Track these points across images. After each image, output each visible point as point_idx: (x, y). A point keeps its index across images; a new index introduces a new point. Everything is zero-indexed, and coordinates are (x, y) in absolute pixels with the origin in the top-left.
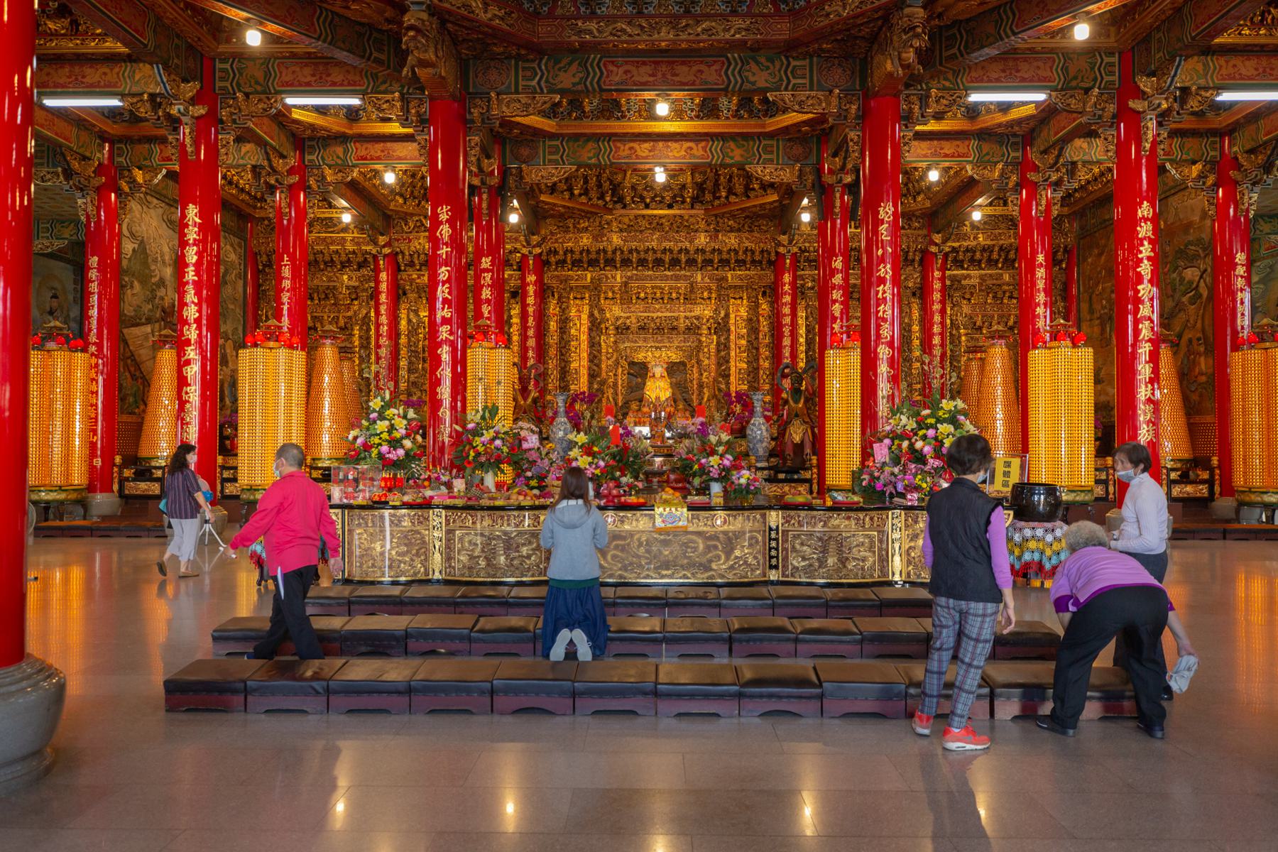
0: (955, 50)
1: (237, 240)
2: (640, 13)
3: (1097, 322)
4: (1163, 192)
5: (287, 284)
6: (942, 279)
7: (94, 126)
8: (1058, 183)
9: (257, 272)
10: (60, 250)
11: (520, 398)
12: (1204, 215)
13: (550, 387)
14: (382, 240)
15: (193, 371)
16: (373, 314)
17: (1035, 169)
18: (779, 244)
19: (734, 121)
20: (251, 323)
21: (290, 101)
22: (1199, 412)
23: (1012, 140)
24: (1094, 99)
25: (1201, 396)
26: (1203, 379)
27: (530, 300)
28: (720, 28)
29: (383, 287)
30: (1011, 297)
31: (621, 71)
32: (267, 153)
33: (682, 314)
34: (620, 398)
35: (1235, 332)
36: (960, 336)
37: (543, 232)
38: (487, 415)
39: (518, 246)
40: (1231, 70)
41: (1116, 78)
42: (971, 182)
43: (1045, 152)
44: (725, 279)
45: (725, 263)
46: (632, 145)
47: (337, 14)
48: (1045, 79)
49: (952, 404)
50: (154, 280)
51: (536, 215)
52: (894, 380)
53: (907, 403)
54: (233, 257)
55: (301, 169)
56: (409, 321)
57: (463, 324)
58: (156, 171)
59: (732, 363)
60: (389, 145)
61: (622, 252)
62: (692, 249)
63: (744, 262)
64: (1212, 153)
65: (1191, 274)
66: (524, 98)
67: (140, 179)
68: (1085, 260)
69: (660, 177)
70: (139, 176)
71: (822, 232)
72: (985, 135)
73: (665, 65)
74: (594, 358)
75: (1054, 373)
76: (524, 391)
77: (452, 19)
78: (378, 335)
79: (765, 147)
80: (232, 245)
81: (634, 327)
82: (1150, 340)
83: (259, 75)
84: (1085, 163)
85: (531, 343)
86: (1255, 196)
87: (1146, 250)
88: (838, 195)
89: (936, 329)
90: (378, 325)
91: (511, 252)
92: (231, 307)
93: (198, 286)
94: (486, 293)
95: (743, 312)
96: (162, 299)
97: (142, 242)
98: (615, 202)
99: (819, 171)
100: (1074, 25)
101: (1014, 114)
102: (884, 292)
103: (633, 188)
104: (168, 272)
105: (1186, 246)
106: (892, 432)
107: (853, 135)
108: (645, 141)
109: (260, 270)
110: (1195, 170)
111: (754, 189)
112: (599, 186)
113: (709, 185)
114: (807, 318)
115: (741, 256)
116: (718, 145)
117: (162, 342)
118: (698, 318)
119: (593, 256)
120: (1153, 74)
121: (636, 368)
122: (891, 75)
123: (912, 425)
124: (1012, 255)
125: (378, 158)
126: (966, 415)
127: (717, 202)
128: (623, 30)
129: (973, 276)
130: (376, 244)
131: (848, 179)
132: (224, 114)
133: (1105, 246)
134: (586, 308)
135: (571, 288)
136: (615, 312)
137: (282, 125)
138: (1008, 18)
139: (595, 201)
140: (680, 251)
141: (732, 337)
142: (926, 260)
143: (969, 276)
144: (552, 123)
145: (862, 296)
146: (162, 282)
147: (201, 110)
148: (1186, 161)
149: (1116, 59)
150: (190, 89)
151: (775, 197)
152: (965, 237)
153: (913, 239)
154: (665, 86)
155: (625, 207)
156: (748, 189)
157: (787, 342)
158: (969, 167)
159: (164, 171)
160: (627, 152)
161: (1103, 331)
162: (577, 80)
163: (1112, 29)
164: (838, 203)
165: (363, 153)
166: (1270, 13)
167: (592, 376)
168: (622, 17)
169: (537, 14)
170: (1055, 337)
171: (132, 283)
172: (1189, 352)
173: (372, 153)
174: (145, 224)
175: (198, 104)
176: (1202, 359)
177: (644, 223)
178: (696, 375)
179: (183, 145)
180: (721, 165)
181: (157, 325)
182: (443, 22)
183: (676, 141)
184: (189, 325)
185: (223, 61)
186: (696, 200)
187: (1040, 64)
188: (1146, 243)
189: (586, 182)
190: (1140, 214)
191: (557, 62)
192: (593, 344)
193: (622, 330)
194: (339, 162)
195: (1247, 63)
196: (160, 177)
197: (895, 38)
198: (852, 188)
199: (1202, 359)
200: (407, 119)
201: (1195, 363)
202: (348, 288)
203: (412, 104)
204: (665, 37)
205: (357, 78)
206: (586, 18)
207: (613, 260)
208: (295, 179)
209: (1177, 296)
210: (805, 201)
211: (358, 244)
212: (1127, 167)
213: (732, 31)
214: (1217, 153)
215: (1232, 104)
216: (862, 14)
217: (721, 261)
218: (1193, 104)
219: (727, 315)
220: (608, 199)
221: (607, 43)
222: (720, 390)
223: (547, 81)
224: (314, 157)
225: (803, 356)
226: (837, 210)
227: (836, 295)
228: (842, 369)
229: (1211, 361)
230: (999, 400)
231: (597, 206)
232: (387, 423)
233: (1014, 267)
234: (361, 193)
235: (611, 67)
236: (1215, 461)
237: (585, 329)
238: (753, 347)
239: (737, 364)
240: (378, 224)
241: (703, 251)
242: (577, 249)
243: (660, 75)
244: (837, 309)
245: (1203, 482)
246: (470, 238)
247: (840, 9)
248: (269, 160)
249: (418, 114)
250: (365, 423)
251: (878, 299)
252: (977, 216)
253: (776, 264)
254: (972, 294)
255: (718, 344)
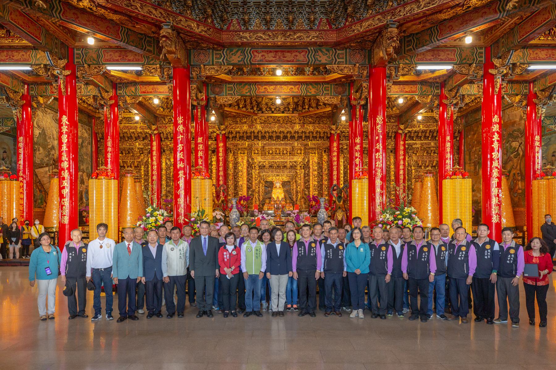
0: (411, 47)
1: (88, 127)
2: (269, 29)
3: (473, 164)
4: (502, 107)
5: (109, 149)
6: (404, 145)
7: (20, 77)
8: (456, 104)
9: (97, 142)
10: (6, 131)
11: (216, 200)
12: (521, 118)
13: (230, 193)
14: (154, 127)
15: (66, 191)
16: (150, 160)
17: (446, 98)
18: (332, 129)
19: (311, 76)
20: (94, 164)
21: (109, 68)
22: (518, 206)
23: (436, 85)
24: (473, 69)
25: (519, 199)
26: (520, 191)
27: (221, 154)
28: (305, 36)
29: (154, 148)
30: (435, 153)
31: (260, 55)
32: (99, 90)
33: (288, 160)
34: (261, 197)
35: (535, 172)
36: (412, 170)
37: (226, 124)
38: (200, 214)
39: (215, 130)
40: (535, 56)
41: (483, 59)
42: (417, 103)
43: (451, 90)
44: (307, 145)
45: (307, 138)
46: (265, 87)
47: (130, 30)
48: (451, 59)
49: (410, 209)
50: (49, 147)
51: (223, 116)
52: (382, 188)
53: (389, 208)
54: (86, 135)
55: (115, 97)
56: (166, 163)
57: (189, 162)
58: (48, 97)
59: (311, 182)
60: (155, 86)
61: (262, 133)
62: (293, 132)
63: (316, 137)
64: (525, 91)
65: (515, 144)
66: (216, 67)
67: (42, 101)
68: (467, 136)
69: (278, 102)
70: (41, 100)
71: (351, 125)
72: (423, 83)
73: (281, 52)
74: (249, 180)
75: (454, 190)
76: (218, 197)
77: (182, 32)
78: (152, 170)
79: (326, 88)
80: (85, 130)
81: (267, 166)
82: (497, 177)
83: (95, 56)
84: (468, 95)
85: (221, 173)
86: (544, 110)
87: (496, 137)
88: (358, 110)
89: (401, 167)
90: (152, 166)
91: (212, 133)
92: (86, 157)
93: (68, 153)
94: (200, 154)
95: (316, 160)
96: (53, 155)
97: (43, 129)
98: (258, 110)
99: (350, 99)
100: (465, 37)
101: (437, 74)
102: (379, 156)
103: (266, 104)
104: (56, 143)
105: (513, 132)
106: (382, 221)
107: (364, 84)
108: (271, 85)
109: (98, 141)
110: (518, 98)
111: (320, 105)
112: (251, 103)
113: (300, 103)
114: (344, 162)
115: (315, 135)
116: (304, 87)
117: (51, 177)
118: (295, 162)
119: (249, 135)
120: (500, 58)
121: (268, 184)
122: (382, 58)
123: (391, 218)
124: (435, 134)
125: (151, 92)
126: (415, 214)
127: (304, 111)
128: (261, 37)
129: (418, 144)
130: (151, 129)
131: (363, 103)
132: (78, 74)
133: (477, 130)
134: (246, 158)
135: (239, 149)
136: (258, 159)
137: (106, 78)
138: (435, 33)
139: (249, 110)
140: (288, 132)
141: (311, 170)
142: (397, 136)
143: (416, 144)
144: (230, 77)
145: (369, 152)
146: (53, 147)
147: (68, 72)
148: (513, 94)
149: (483, 51)
150: (63, 63)
151: (330, 109)
152: (414, 126)
153: (391, 127)
154: (281, 62)
155: (263, 113)
156: (318, 105)
157: (335, 173)
158: (416, 97)
159: (53, 98)
160: (263, 90)
161: (475, 168)
162: (240, 59)
163: (482, 37)
164: (358, 113)
165: (144, 90)
166: (553, 29)
167: (249, 188)
168: (260, 31)
169: (221, 29)
170: (454, 173)
171: (39, 148)
172: (514, 179)
173: (148, 90)
174: (45, 122)
175: (66, 70)
176: (520, 182)
177: (271, 120)
178: (295, 187)
179: (60, 89)
180: (305, 96)
181: (51, 167)
182: (179, 33)
183: (286, 85)
184: (64, 170)
185: (78, 49)
186: (295, 110)
187: (449, 53)
188: (496, 134)
189: (245, 101)
190: (493, 121)
191: (231, 51)
192: (249, 174)
193: (262, 167)
194: (133, 94)
195: (542, 52)
196: (51, 100)
197: (384, 42)
198: (364, 107)
199: (520, 182)
200: (163, 77)
201: (516, 184)
202: (138, 148)
203: (165, 70)
204: (280, 40)
205: (140, 58)
206: (244, 32)
207: (258, 136)
208: (113, 102)
209: (508, 154)
210: (343, 112)
211: (143, 129)
212: (488, 98)
213: (310, 38)
214: (528, 91)
215: (533, 71)
216: (369, 31)
217: (306, 137)
218: (518, 71)
219: (309, 161)
220: (255, 109)
221: (254, 43)
222: (305, 194)
223: (226, 60)
224: (121, 92)
225: (342, 179)
226: (358, 116)
227: (357, 154)
228: (360, 188)
229: (523, 184)
230: (430, 201)
231: (250, 112)
232: (154, 218)
233: (436, 140)
234: (143, 107)
235: (256, 54)
236: (525, 228)
237: (245, 167)
238: (320, 175)
239: (313, 182)
240: (152, 120)
241: (298, 132)
242: (241, 132)
243: (278, 57)
244: (357, 161)
245: (520, 237)
246: (192, 127)
247: (359, 28)
248: (101, 94)
249: (168, 75)
250: (144, 218)
251: (376, 159)
252: (420, 118)
253: (330, 138)
254: (417, 151)
255: (305, 174)
